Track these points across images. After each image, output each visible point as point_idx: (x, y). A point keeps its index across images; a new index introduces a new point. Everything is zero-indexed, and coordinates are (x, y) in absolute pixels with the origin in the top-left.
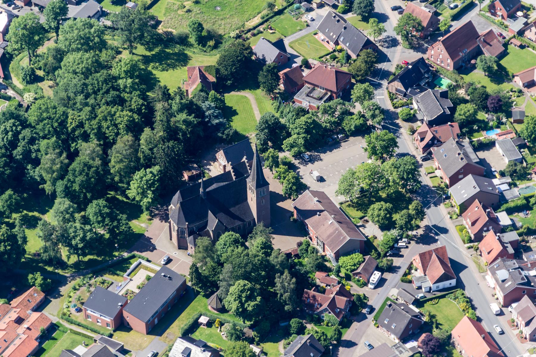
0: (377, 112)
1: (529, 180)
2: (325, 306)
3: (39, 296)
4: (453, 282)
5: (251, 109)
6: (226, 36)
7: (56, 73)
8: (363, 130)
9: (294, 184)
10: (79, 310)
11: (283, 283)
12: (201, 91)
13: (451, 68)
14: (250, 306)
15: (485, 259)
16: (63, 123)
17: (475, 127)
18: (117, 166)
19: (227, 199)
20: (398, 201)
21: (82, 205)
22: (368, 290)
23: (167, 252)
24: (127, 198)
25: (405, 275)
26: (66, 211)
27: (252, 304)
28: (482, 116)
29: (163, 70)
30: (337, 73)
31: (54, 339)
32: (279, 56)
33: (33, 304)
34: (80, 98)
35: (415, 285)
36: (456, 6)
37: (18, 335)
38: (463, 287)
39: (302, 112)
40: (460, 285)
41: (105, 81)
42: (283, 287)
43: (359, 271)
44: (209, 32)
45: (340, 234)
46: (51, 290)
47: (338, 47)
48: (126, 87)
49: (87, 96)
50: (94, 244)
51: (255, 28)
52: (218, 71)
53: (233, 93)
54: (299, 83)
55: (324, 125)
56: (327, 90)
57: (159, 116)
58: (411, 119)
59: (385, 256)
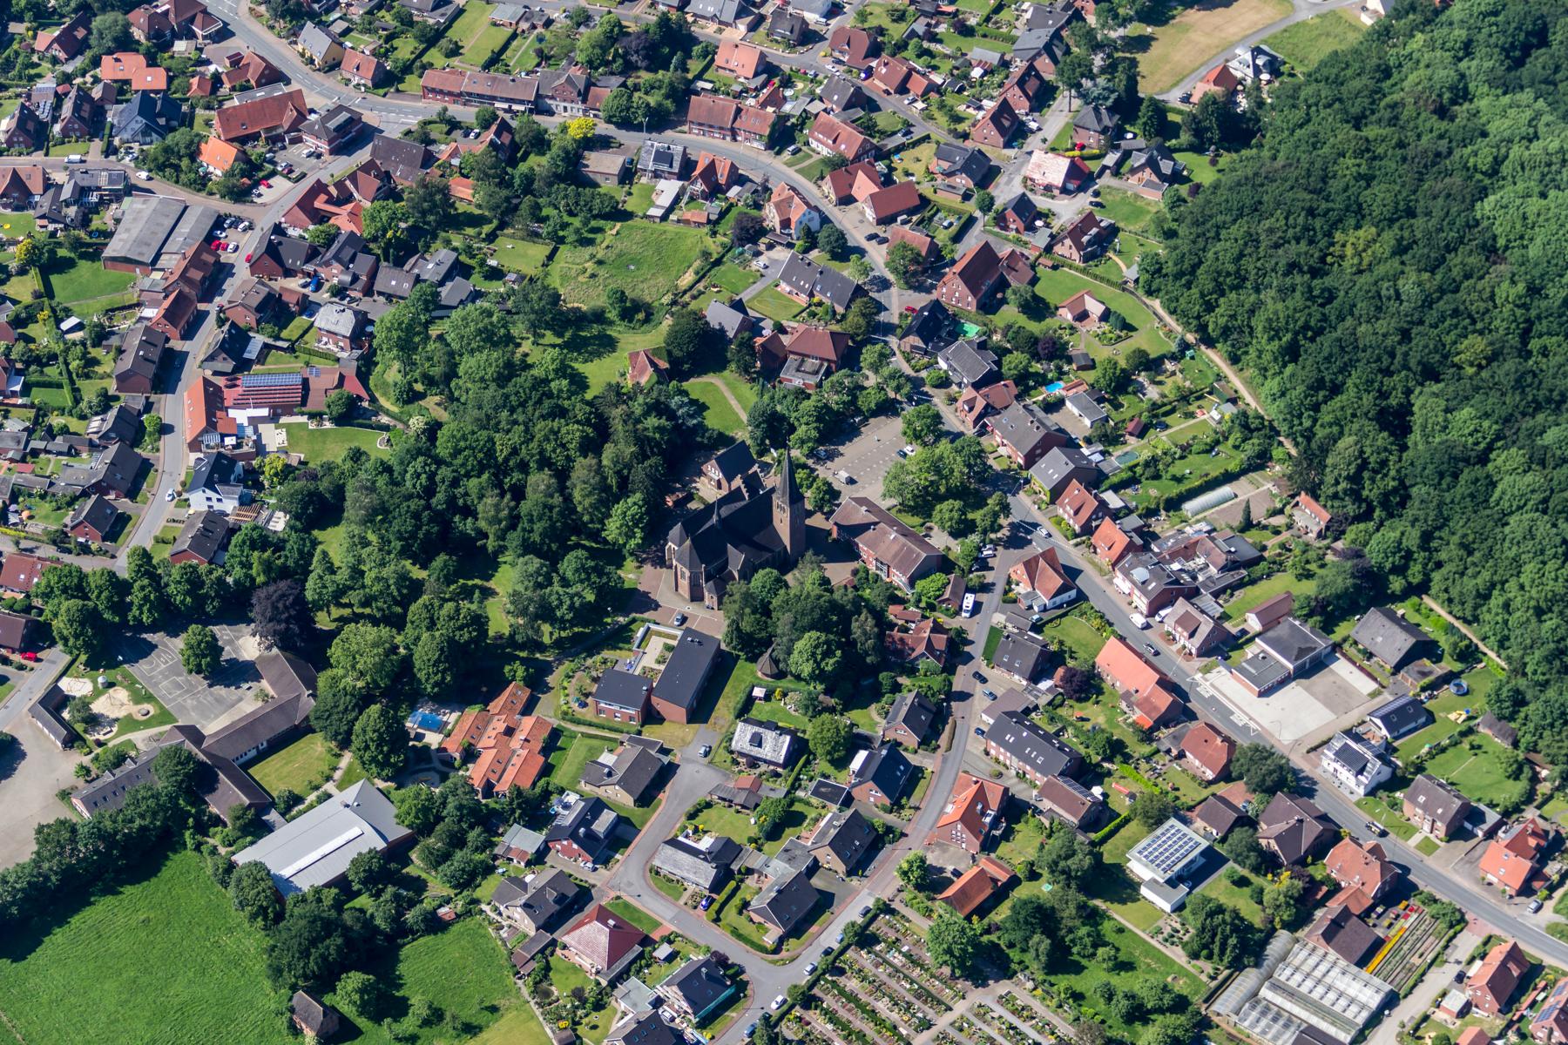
0: (902, 380)
1: (1125, 443)
2: (921, 649)
3: (524, 694)
4: (1073, 593)
5: (729, 400)
6: (656, 304)
7: (453, 385)
8: (888, 408)
9: (826, 492)
10: (584, 705)
11: (862, 626)
12: (658, 382)
13: (973, 308)
14: (829, 665)
15: (1104, 558)
16: (490, 453)
17: (1032, 383)
18: (587, 503)
19: (745, 523)
20: (971, 496)
21: (553, 559)
22: (962, 621)
23: (677, 610)
24: (605, 541)
25: (1006, 592)
26: (538, 573)
27: (832, 661)
28: (1037, 367)
29: (586, 361)
30: (832, 334)
31: (561, 749)
32: (743, 321)
33: (519, 707)
34: (505, 414)
35: (1023, 605)
36: (951, 224)
37: (514, 751)
38: (1086, 599)
39: (802, 394)
40: (1082, 596)
41: (534, 388)
42: (865, 633)
43: (947, 596)
44: (633, 301)
45: (910, 551)
46: (537, 683)
47: (816, 300)
48: (560, 391)
49: (512, 411)
50: (585, 614)
51: (691, 288)
52: (669, 353)
53: (692, 380)
54: (781, 355)
55: (835, 407)
56: (822, 359)
57: (617, 426)
58: (944, 383)
59: (971, 572)
